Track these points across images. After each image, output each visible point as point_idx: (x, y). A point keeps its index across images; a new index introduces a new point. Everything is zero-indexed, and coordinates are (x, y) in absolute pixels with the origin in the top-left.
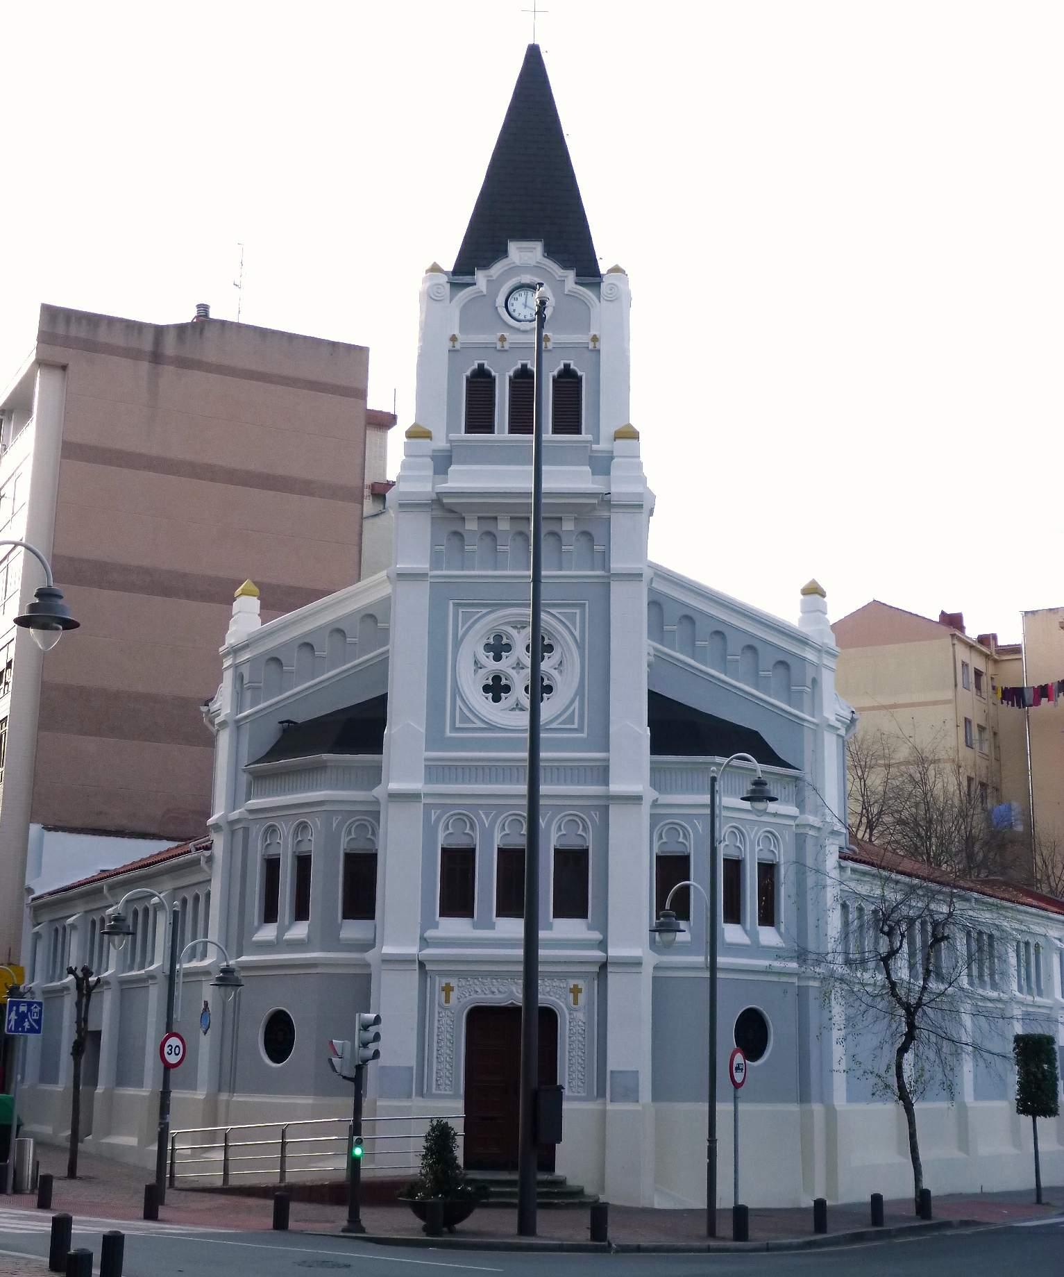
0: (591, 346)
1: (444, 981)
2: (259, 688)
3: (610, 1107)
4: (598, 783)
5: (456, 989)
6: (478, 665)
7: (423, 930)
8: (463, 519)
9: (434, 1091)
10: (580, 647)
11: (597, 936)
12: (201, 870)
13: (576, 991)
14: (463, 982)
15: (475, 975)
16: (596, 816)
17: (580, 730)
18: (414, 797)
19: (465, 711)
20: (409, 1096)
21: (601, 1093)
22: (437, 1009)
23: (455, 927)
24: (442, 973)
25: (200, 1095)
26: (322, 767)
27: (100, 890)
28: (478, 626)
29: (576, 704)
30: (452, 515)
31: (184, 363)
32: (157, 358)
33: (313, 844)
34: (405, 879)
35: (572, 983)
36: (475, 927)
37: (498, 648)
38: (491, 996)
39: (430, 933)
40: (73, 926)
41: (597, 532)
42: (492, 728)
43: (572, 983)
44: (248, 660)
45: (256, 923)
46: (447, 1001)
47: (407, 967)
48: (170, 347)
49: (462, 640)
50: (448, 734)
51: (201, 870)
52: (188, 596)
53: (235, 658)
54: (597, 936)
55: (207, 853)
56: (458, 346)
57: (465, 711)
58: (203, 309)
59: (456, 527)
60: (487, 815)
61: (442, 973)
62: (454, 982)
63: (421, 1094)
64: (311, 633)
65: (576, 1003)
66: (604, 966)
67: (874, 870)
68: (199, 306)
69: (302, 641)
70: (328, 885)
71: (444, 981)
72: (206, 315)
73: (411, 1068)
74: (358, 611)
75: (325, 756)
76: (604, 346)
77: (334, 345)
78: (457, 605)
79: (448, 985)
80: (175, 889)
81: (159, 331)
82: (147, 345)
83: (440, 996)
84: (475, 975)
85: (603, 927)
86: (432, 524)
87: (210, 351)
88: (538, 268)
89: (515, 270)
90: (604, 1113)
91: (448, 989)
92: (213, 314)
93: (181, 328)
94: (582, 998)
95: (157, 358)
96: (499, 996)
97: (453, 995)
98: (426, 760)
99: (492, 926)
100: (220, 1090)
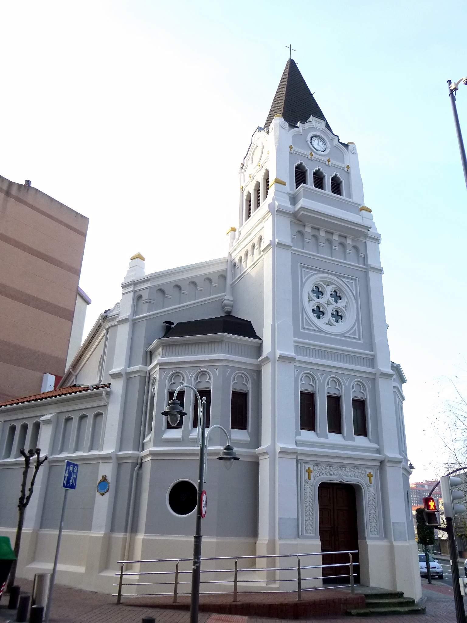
0: (346, 170)
1: (307, 466)
2: (153, 303)
3: (395, 544)
4: (369, 367)
6: (310, 300)
8: (304, 226)
10: (356, 299)
11: (375, 446)
12: (103, 399)
15: (323, 464)
17: (360, 340)
18: (290, 359)
19: (308, 320)
22: (304, 483)
23: (308, 435)
24: (306, 462)
25: (98, 532)
26: (220, 341)
27: (100, 394)
28: (311, 279)
29: (356, 326)
30: (300, 223)
31: (18, 200)
32: (8, 193)
33: (211, 384)
34: (277, 406)
35: (368, 471)
37: (318, 292)
39: (298, 438)
40: (47, 422)
41: (361, 248)
43: (368, 471)
44: (148, 288)
45: (163, 429)
46: (309, 479)
47: (291, 457)
48: (14, 191)
49: (305, 283)
50: (301, 331)
51: (103, 399)
52: (6, 296)
53: (134, 288)
55: (108, 389)
56: (292, 152)
57: (308, 320)
58: (28, 182)
59: (301, 229)
60: (322, 375)
61: (306, 462)
62: (312, 467)
64: (181, 280)
68: (26, 181)
69: (192, 280)
70: (221, 408)
71: (307, 466)
72: (29, 185)
74: (189, 278)
75: (225, 334)
76: (352, 171)
77: (77, 213)
78: (301, 266)
80: (59, 413)
81: (11, 184)
82: (5, 187)
84: (323, 464)
86: (291, 225)
87: (30, 199)
88: (321, 131)
89: (312, 129)
90: (392, 548)
91: (309, 471)
92: (32, 185)
93: (20, 186)
95: (8, 193)
96: (333, 477)
97: (312, 475)
98: (295, 342)
100: (112, 530)
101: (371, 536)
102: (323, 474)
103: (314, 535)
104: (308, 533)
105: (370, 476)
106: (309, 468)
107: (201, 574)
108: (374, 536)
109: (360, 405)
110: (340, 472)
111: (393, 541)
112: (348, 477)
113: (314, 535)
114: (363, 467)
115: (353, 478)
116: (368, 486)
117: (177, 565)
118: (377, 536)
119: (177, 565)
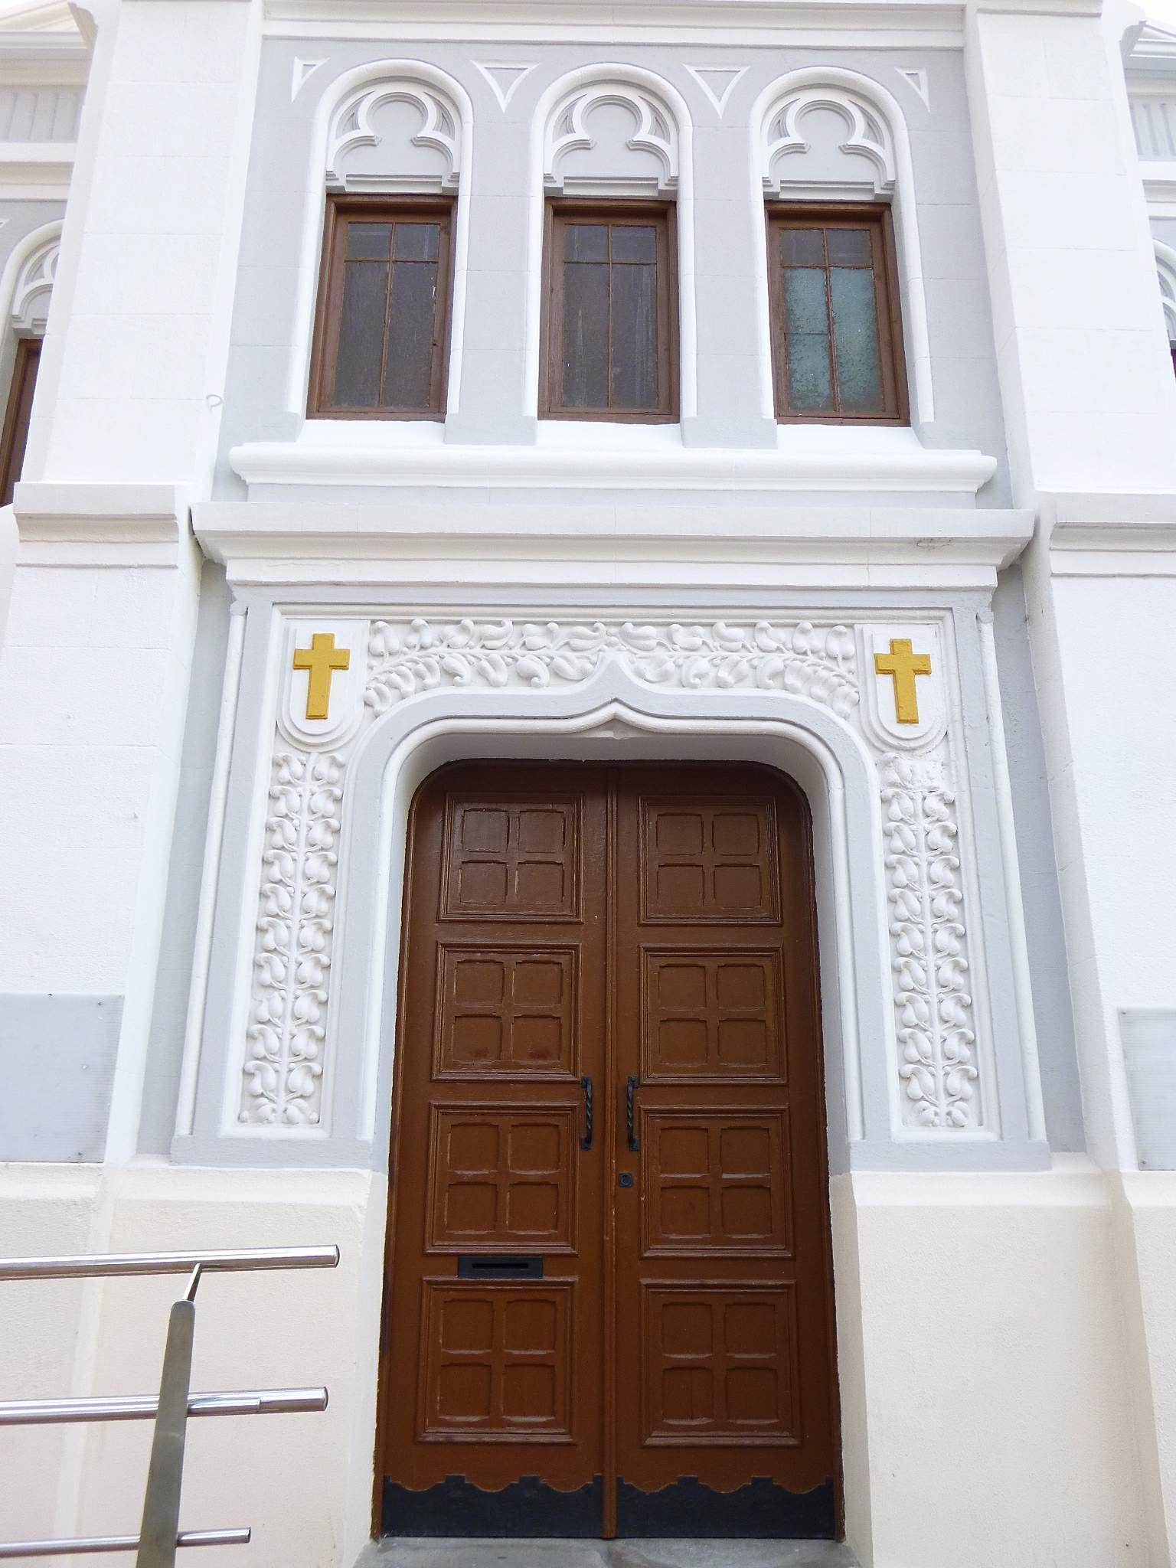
3: (1144, 1194)
5: (358, 661)
7: (229, 436)
9: (229, 1127)
13: (901, 667)
14: (395, 637)
15: (448, 607)
16: (960, 669)
20: (87, 1151)
21: (1071, 1128)
22: (266, 747)
36: (446, 439)
38: (778, 693)
42: (650, 105)
43: (880, 636)
54: (980, 461)
61: (295, 600)
62: (349, 634)
63: (159, 1138)
65: (907, 717)
66: (1016, 569)
67: (957, 701)
73: (111, 1008)
79: (322, 641)
83: (283, 693)
85: (991, 420)
90: (1113, 1237)
91: (320, 663)
94: (931, 695)
97: (929, 693)
99: (529, 438)
101: (902, 1129)
102: (451, 674)
103: (318, 1134)
104: (262, 1120)
105: (901, 667)
106: (898, 647)
107: (158, 1391)
108: (943, 1135)
109: (836, 237)
110: (622, 658)
111: (1127, 1166)
112: (683, 688)
113: (318, 1134)
114: (838, 610)
115: (746, 691)
116: (879, 744)
117: (183, 1315)
118: (974, 1134)
119: (183, 1315)
